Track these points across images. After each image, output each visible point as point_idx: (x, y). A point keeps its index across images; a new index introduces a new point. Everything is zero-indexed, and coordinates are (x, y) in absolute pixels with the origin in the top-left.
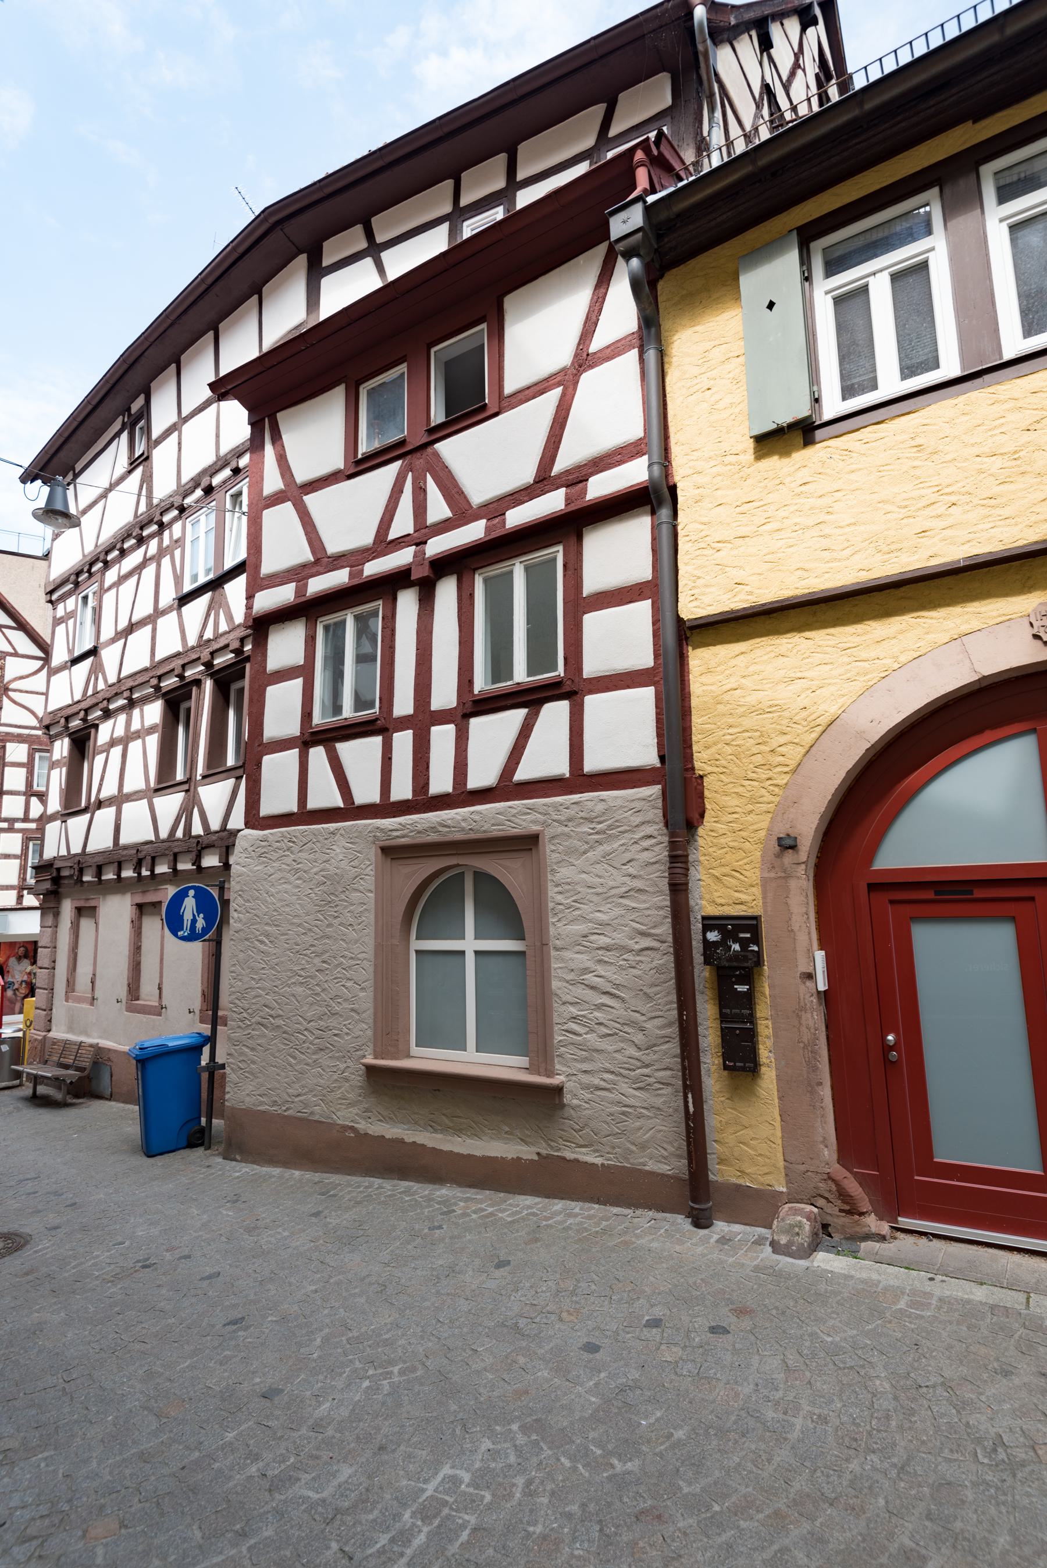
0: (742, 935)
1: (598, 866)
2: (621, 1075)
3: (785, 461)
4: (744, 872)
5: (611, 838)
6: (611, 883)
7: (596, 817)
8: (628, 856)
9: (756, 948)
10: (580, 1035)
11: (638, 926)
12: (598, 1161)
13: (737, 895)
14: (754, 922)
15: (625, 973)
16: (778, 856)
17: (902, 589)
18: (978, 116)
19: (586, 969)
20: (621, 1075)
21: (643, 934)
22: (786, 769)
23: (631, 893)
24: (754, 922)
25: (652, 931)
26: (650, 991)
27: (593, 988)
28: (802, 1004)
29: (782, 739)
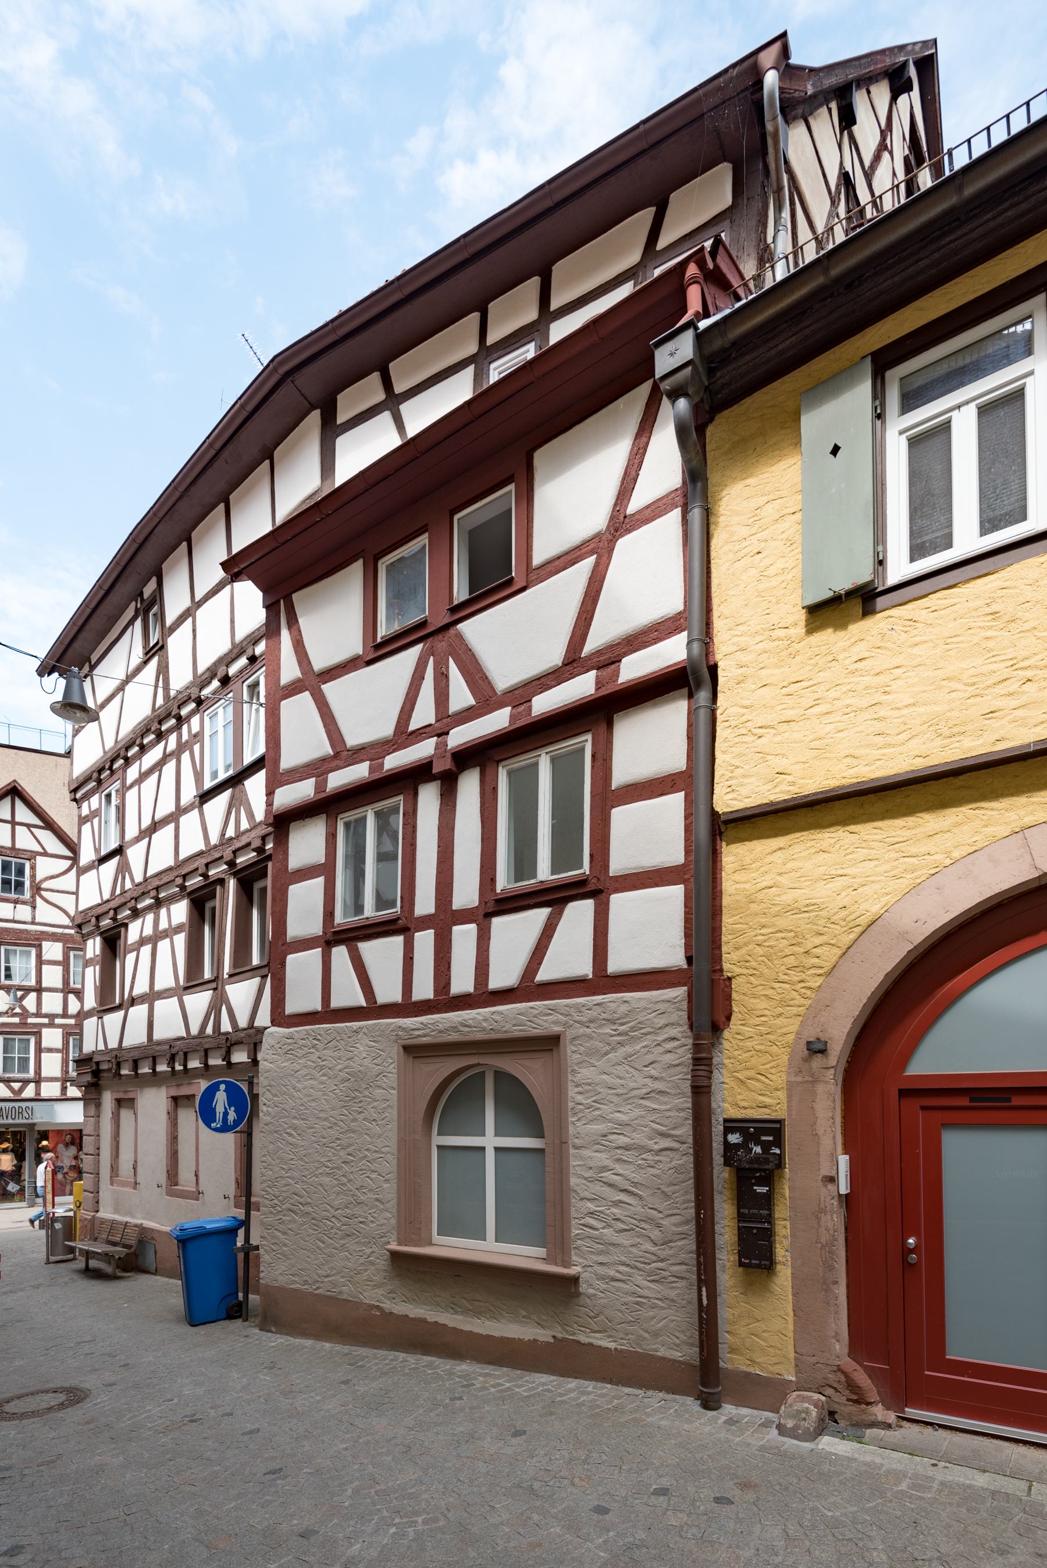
0: (764, 1138)
1: (619, 1068)
2: (636, 1268)
4: (769, 1076)
6: (632, 1085)
8: (650, 1058)
9: (778, 1151)
10: (597, 1230)
11: (658, 1127)
12: (612, 1346)
13: (761, 1098)
14: (778, 1126)
15: (643, 1171)
16: (806, 1060)
20: (636, 1268)
21: (663, 1135)
24: (778, 1126)
25: (673, 1132)
28: (822, 1206)
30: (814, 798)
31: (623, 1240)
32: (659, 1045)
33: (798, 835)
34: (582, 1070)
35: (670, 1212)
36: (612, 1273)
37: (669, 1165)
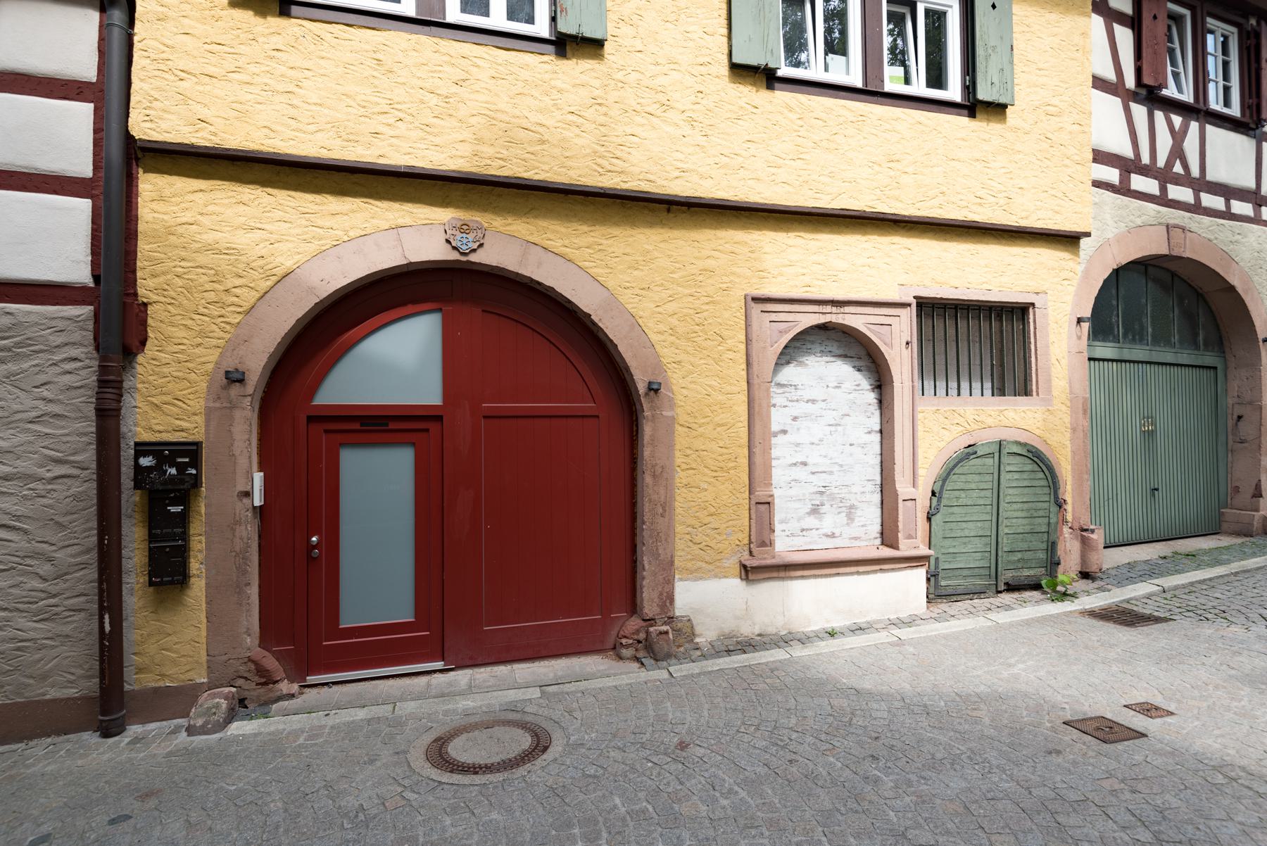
2: (18, 610)
3: (259, 20)
5: (18, 357)
6: (16, 407)
8: (42, 378)
11: (53, 453)
13: (178, 422)
20: (18, 610)
25: (72, 458)
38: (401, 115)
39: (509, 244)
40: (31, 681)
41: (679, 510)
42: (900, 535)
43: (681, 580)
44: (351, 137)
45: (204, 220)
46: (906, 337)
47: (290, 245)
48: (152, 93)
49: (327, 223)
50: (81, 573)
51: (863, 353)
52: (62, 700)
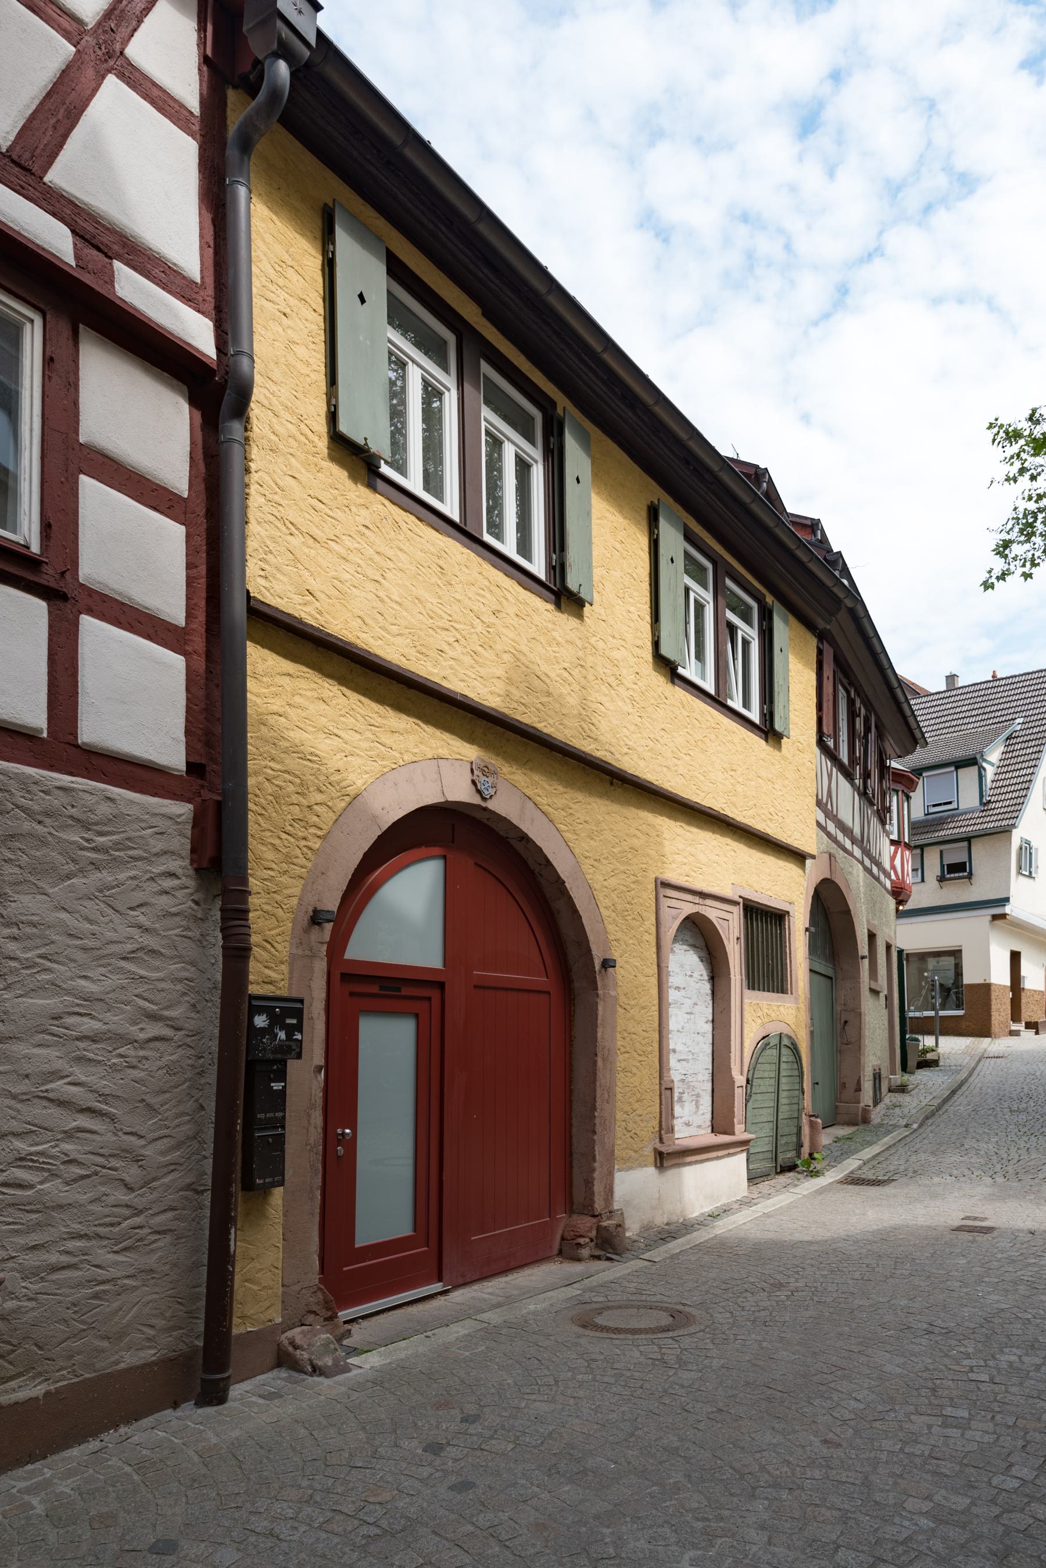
0: (289, 1021)
1: (89, 904)
2: (100, 1237)
3: (349, 484)
4: (276, 945)
5: (117, 863)
6: (110, 935)
7: (96, 824)
8: (139, 897)
9: (299, 1037)
10: (31, 1186)
11: (147, 1004)
12: (38, 1390)
13: (267, 971)
14: (299, 1005)
15: (119, 1076)
16: (307, 931)
17: (412, 691)
18: (489, 314)
19: (53, 1073)
20: (100, 1237)
21: (153, 1017)
22: (320, 833)
23: (140, 954)
24: (299, 1005)
25: (166, 1013)
26: (154, 1101)
27: (61, 1103)
28: (313, 1101)
29: (320, 798)
30: (334, 641)
31: (79, 1195)
32: (152, 879)
33: (306, 669)
34: (21, 897)
35: (157, 1134)
36: (54, 1258)
37: (158, 1063)
38: (459, 637)
39: (528, 801)
40: (105, 1344)
41: (619, 1096)
42: (735, 1120)
43: (619, 1170)
44: (424, 650)
45: (292, 712)
46: (737, 934)
47: (360, 761)
48: (268, 542)
49: (388, 739)
50: (170, 1177)
51: (703, 944)
52: (138, 1367)
